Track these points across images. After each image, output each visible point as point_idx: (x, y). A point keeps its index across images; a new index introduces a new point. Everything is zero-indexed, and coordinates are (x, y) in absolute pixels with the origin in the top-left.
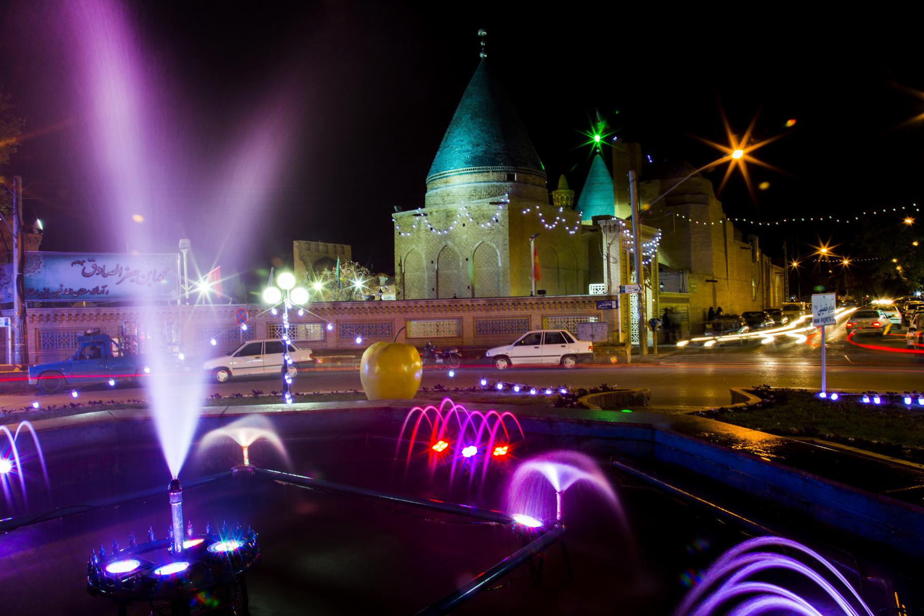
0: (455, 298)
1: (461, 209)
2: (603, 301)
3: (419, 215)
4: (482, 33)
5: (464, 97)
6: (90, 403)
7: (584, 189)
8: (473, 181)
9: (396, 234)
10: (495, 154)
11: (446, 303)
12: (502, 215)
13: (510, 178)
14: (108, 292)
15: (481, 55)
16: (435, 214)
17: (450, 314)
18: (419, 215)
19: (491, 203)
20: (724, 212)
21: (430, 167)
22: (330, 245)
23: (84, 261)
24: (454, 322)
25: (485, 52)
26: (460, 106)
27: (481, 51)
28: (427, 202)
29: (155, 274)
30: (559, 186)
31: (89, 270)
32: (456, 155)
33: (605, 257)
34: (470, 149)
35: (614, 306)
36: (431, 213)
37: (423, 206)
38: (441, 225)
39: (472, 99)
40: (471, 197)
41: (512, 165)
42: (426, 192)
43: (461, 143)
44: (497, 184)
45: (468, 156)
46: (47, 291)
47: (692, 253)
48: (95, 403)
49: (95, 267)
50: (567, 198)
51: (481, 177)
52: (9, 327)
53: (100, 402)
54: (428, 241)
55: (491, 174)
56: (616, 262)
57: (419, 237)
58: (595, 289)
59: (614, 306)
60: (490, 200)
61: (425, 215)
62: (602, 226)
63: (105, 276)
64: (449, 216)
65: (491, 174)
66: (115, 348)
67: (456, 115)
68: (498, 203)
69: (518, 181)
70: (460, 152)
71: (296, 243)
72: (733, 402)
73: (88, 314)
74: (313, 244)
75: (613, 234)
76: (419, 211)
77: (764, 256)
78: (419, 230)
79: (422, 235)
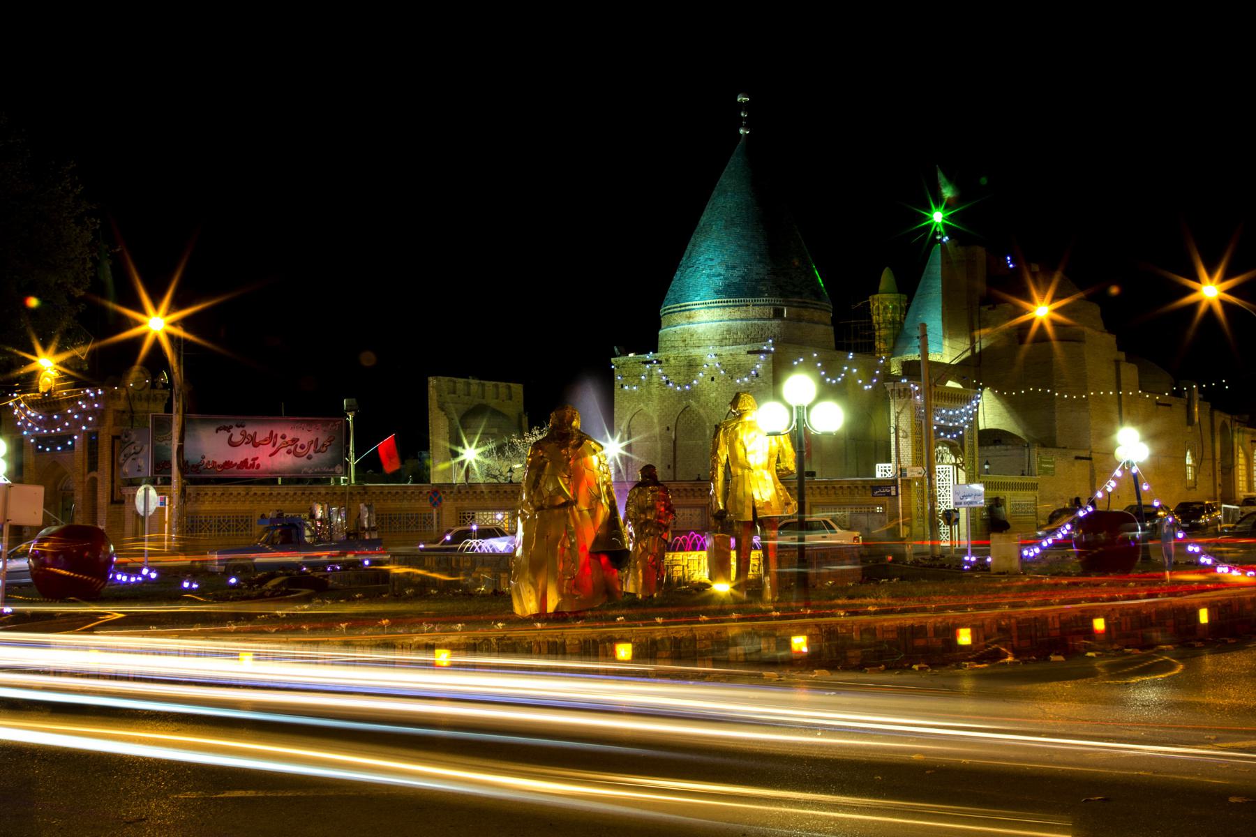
0: (699, 479)
1: (708, 356)
2: (880, 487)
3: (651, 362)
4: (741, 98)
5: (715, 193)
7: (918, 291)
8: (725, 318)
9: (617, 387)
10: (757, 281)
11: (686, 485)
12: (764, 368)
13: (778, 314)
14: (258, 466)
15: (742, 131)
16: (672, 362)
17: (691, 501)
18: (651, 362)
19: (749, 352)
20: (1120, 349)
21: (665, 293)
22: (489, 384)
24: (698, 511)
25: (746, 127)
26: (709, 206)
27: (741, 126)
28: (661, 344)
29: (316, 446)
30: (882, 286)
31: (237, 437)
32: (703, 280)
33: (892, 430)
34: (722, 272)
35: (893, 493)
36: (667, 360)
37: (655, 351)
38: (681, 378)
39: (726, 202)
40: (722, 342)
41: (781, 295)
42: (660, 328)
43: (709, 263)
44: (759, 322)
45: (719, 282)
47: (1057, 415)
49: (244, 435)
50: (895, 308)
51: (737, 313)
54: (662, 399)
55: (750, 308)
56: (906, 437)
57: (649, 393)
58: (883, 471)
60: (748, 347)
61: (659, 362)
62: (889, 389)
63: (256, 445)
64: (692, 366)
65: (750, 308)
66: (307, 533)
67: (704, 219)
68: (759, 352)
69: (789, 319)
70: (708, 276)
71: (432, 381)
73: (235, 493)
74: (460, 382)
75: (904, 400)
76: (649, 356)
77: (1216, 413)
78: (649, 383)
79: (655, 390)
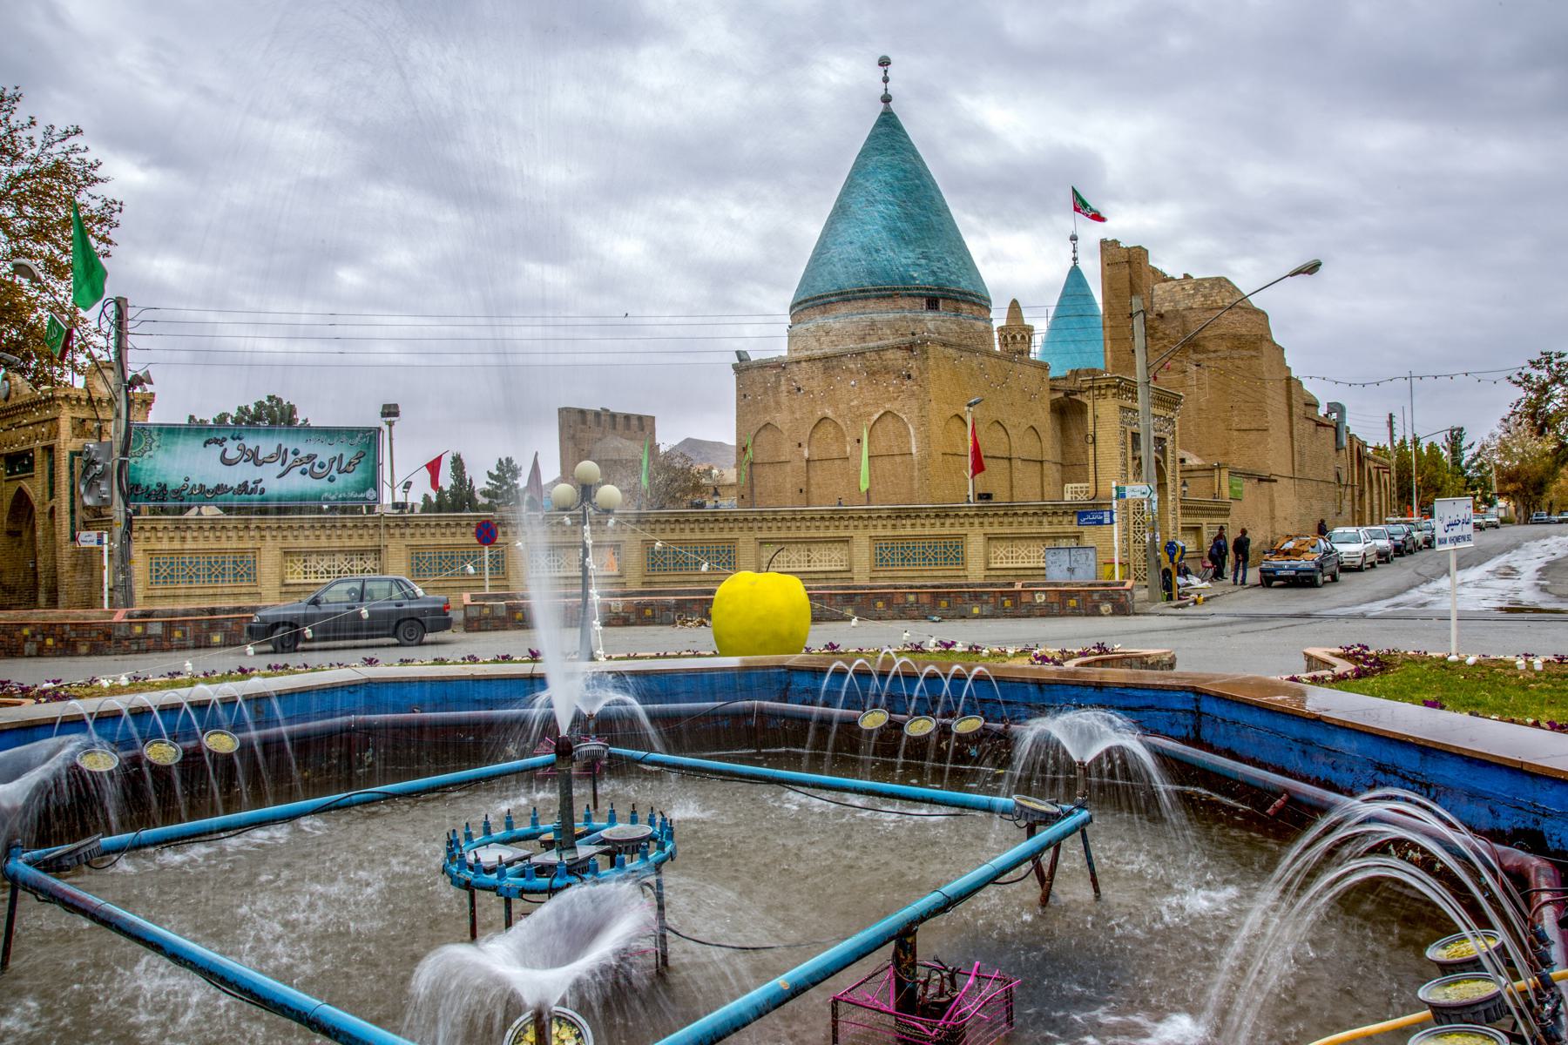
6: (269, 667)
14: (263, 491)
23: (225, 439)
35: (1107, 520)
46: (163, 488)
48: (276, 667)
49: (243, 450)
52: (106, 548)
53: (286, 666)
59: (1107, 520)
72: (1309, 669)
